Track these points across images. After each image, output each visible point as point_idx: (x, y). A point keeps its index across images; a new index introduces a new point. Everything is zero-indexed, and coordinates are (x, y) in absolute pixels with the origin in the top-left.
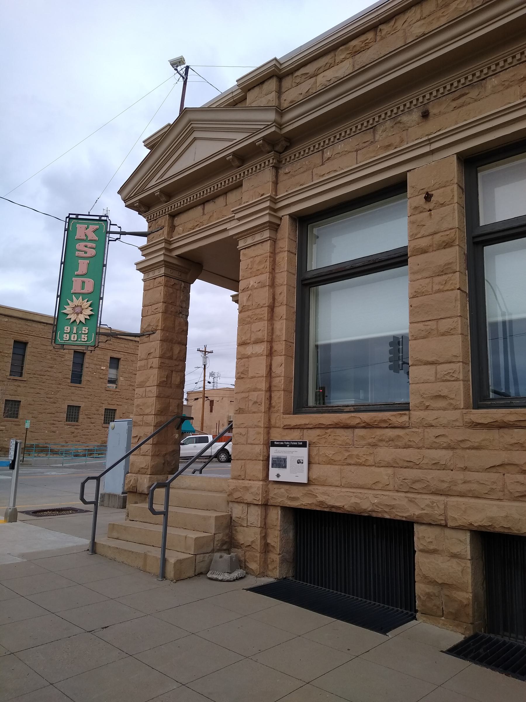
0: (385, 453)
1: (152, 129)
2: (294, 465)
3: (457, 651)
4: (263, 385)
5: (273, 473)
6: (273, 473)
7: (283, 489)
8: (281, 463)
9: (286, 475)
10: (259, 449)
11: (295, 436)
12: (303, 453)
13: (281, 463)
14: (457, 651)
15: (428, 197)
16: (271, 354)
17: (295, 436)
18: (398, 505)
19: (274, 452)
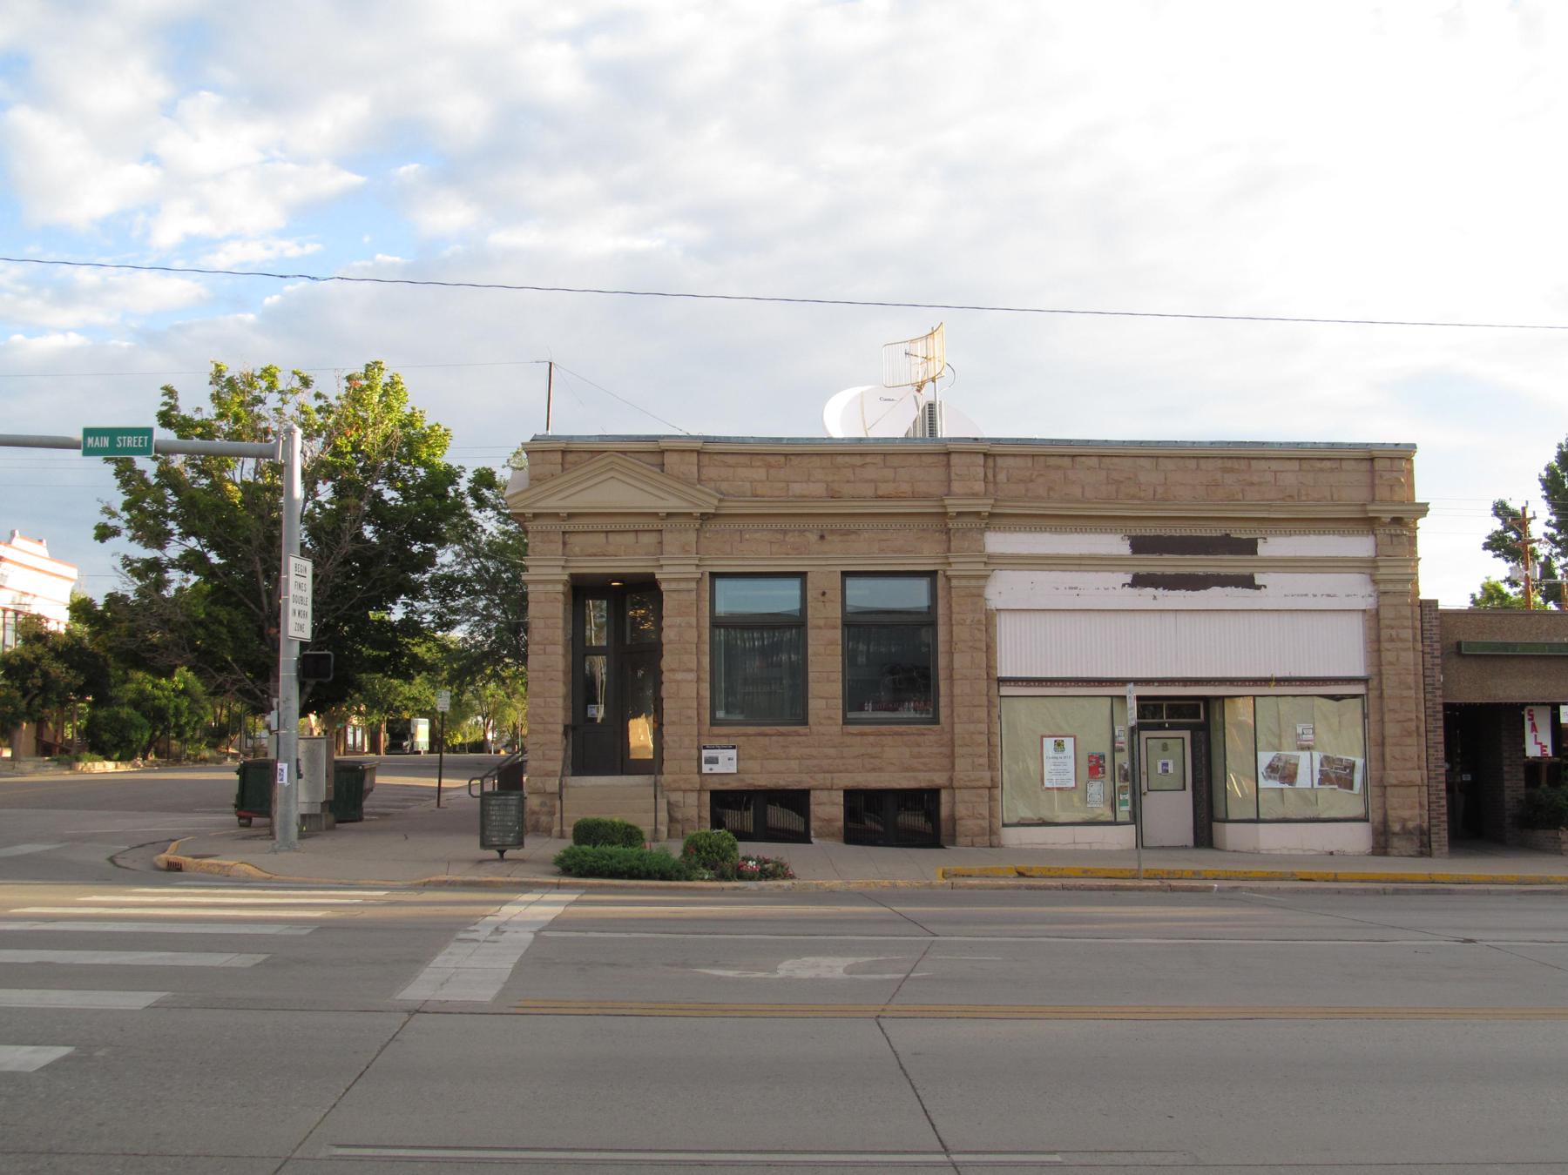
0: (793, 751)
1: (579, 420)
2: (725, 764)
3: (1473, 596)
4: (695, 705)
5: (1049, 744)
6: (706, 768)
7: (715, 779)
8: (1059, 745)
9: (717, 769)
10: (695, 752)
11: (724, 742)
12: (733, 753)
13: (714, 761)
14: (1473, 596)
15: (824, 594)
16: (699, 680)
17: (724, 742)
18: (804, 781)
19: (705, 753)
